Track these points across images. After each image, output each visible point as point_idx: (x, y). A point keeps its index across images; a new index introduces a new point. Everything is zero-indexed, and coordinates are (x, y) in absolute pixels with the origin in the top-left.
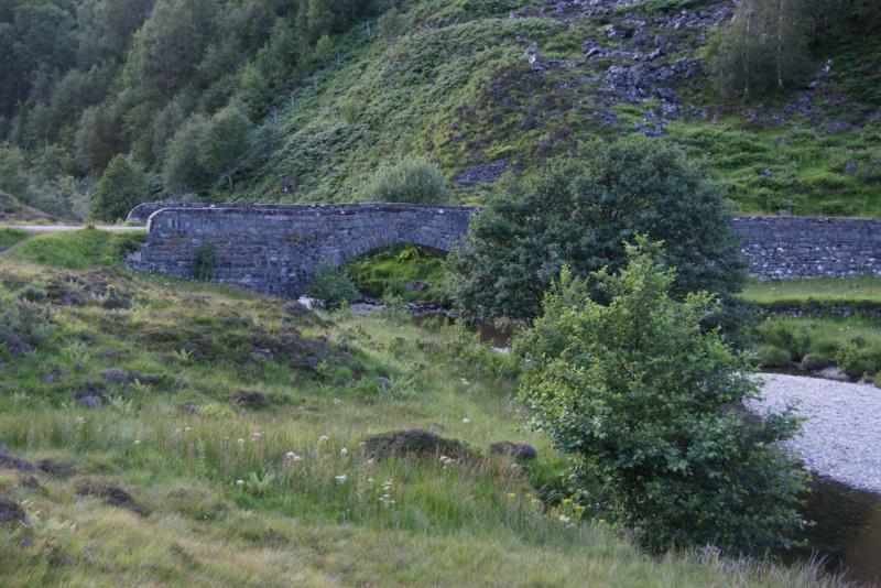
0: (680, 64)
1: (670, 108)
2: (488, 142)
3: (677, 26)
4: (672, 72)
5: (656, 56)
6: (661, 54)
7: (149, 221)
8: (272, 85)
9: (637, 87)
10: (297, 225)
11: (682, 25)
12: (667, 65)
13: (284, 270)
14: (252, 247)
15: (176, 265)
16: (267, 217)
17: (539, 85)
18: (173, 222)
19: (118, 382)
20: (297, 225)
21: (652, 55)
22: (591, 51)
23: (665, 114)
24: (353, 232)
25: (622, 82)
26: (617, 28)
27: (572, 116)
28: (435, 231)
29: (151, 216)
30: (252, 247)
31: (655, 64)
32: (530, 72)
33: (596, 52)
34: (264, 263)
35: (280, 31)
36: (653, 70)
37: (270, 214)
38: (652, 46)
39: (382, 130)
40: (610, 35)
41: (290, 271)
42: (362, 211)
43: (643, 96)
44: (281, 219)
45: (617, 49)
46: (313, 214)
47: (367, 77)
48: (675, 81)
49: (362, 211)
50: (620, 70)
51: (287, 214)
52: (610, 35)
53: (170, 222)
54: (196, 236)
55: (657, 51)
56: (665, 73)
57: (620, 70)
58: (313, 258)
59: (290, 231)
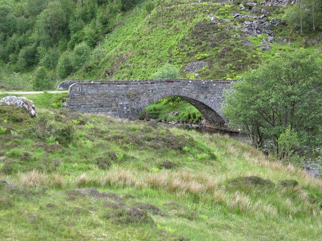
0: (273, 20)
1: (270, 38)
2: (196, 53)
3: (270, 5)
4: (270, 24)
5: (263, 17)
6: (265, 17)
7: (69, 89)
8: (97, 33)
9: (257, 30)
10: (131, 89)
11: (272, 5)
12: (268, 20)
13: (125, 108)
14: (112, 98)
15: (80, 107)
16: (118, 86)
17: (216, 29)
18: (79, 89)
19: (154, 209)
20: (131, 89)
21: (261, 17)
22: (236, 15)
23: (269, 40)
24: (153, 91)
25: (250, 27)
26: (245, 6)
27: (232, 41)
28: (188, 90)
29: (70, 87)
30: (112, 98)
31: (262, 21)
32: (211, 24)
33: (238, 16)
34: (117, 105)
35: (100, 13)
36: (262, 23)
37: (119, 84)
38: (261, 13)
39: (143, 49)
40: (242, 9)
41: (128, 108)
42: (157, 82)
43: (259, 33)
44: (124, 86)
45: (248, 14)
46: (137, 84)
47: (135, 26)
48: (272, 27)
49: (157, 82)
50: (249, 23)
51: (126, 84)
52: (242, 9)
53: (78, 89)
54: (89, 94)
55: (263, 15)
56: (267, 24)
57: (249, 23)
58: (137, 103)
59: (128, 92)
